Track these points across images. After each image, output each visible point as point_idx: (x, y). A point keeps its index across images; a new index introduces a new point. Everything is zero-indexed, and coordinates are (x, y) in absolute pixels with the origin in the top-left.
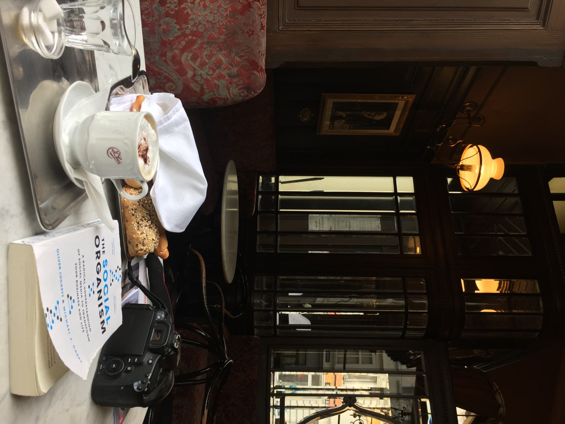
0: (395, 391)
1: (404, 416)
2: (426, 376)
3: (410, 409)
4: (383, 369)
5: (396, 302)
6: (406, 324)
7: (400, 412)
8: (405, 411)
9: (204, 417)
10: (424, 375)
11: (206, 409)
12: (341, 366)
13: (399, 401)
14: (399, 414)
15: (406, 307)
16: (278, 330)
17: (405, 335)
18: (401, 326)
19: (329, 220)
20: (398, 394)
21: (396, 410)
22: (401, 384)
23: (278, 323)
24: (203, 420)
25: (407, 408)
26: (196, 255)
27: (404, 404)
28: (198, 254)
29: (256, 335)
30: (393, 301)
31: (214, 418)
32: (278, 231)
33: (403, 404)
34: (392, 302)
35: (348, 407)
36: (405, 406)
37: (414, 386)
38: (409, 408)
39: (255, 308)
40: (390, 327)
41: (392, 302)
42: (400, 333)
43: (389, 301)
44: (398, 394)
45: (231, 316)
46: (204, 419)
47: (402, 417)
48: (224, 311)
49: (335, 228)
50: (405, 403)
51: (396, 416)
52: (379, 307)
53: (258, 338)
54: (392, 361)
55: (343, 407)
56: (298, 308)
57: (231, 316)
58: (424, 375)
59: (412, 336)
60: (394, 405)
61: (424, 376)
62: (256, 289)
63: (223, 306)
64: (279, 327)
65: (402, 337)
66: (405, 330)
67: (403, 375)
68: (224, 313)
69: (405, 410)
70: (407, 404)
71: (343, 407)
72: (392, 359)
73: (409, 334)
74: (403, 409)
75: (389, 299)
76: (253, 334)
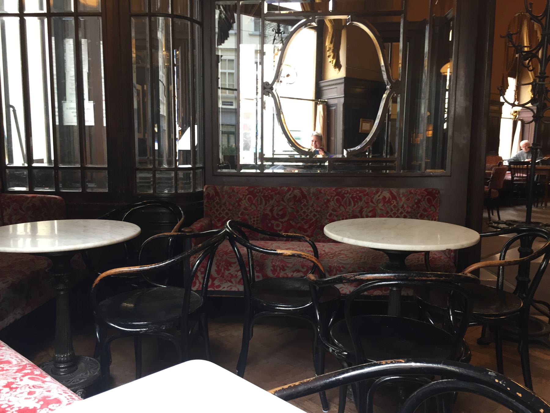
0: (258, 40)
1: (281, 31)
2: (242, 1)
3: (275, 24)
4: (236, 49)
5: (162, 28)
6: (186, 18)
7: (277, 35)
8: (276, 29)
9: (284, 253)
10: (241, 3)
11: (276, 252)
12: (235, 92)
13: (267, 35)
14: (278, 36)
15: (166, 15)
16: (198, 165)
17: (199, 20)
18: (188, 25)
19: (72, 101)
20: (260, 35)
21: (276, 39)
22: (251, 31)
23: (190, 166)
24: (288, 254)
25: (273, 28)
26: (101, 280)
27: (270, 31)
28: (99, 279)
29: (203, 189)
30: (160, 31)
31: (285, 235)
32: (80, 166)
33: (269, 32)
34: (161, 33)
35: (273, 91)
36: (271, 29)
37: (253, 18)
38: (272, 26)
39: (174, 192)
40: (190, 37)
41: (162, 32)
42: (197, 27)
43: (160, 35)
44: (260, 35)
45: (182, 219)
46: (287, 253)
47: (281, 33)
48: (172, 233)
49: (233, 56)
50: (269, 29)
51: (281, 39)
52: (167, 49)
53: (206, 186)
54: (228, 38)
55: (273, 96)
56: (173, 142)
57: (182, 219)
58: (241, 3)
59: (199, 13)
60: (271, 41)
61: (242, 3)
62: (152, 192)
63: (169, 235)
64: (194, 163)
65: (201, 24)
66: (193, 21)
67: (241, 29)
68: (175, 234)
69: (275, 29)
70: (269, 27)
71: (273, 96)
72: (227, 39)
73: (197, 17)
74: (274, 32)
75: (158, 36)
76: (202, 192)
